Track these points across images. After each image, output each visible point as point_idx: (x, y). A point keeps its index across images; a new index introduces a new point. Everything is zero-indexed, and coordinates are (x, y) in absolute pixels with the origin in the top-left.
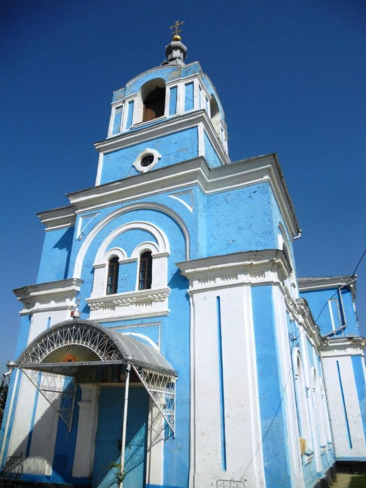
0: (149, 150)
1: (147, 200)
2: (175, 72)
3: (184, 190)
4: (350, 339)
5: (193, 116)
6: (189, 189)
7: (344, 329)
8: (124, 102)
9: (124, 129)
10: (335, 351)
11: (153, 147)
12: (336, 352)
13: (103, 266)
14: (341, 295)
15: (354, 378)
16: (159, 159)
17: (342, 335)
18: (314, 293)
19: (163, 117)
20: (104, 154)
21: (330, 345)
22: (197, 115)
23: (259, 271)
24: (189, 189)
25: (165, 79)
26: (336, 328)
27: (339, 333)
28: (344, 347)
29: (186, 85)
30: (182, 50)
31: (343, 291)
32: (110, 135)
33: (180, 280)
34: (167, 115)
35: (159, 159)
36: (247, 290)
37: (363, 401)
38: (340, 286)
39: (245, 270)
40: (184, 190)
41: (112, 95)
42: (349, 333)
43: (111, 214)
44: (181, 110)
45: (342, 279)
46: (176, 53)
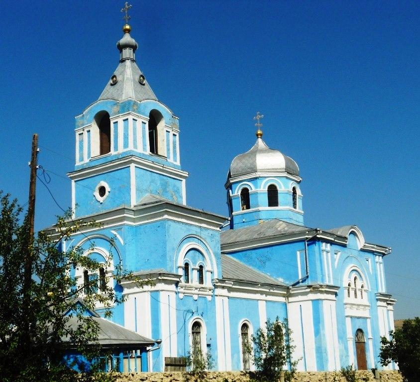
0: (103, 184)
1: (100, 232)
2: (115, 107)
3: (119, 227)
4: (309, 287)
5: (126, 159)
6: (121, 227)
7: (308, 277)
8: (83, 130)
9: (86, 160)
10: (300, 297)
11: (105, 180)
12: (300, 298)
13: (80, 277)
14: (307, 247)
15: (312, 320)
16: (109, 192)
17: (306, 283)
18: (287, 245)
19: (110, 153)
20: (75, 181)
21: (292, 292)
22: (128, 158)
23: (153, 284)
24: (121, 227)
25: (110, 114)
26: (302, 276)
27: (304, 281)
28: (306, 294)
29: (124, 120)
30: (134, 47)
31: (309, 243)
32: (78, 163)
33: (119, 288)
34: (113, 152)
35: (109, 192)
36: (148, 295)
37: (317, 337)
38: (307, 238)
39: (147, 283)
40: (119, 227)
41: (74, 121)
42: (312, 281)
43: (82, 240)
44: (121, 150)
45: (307, 232)
46: (127, 53)
